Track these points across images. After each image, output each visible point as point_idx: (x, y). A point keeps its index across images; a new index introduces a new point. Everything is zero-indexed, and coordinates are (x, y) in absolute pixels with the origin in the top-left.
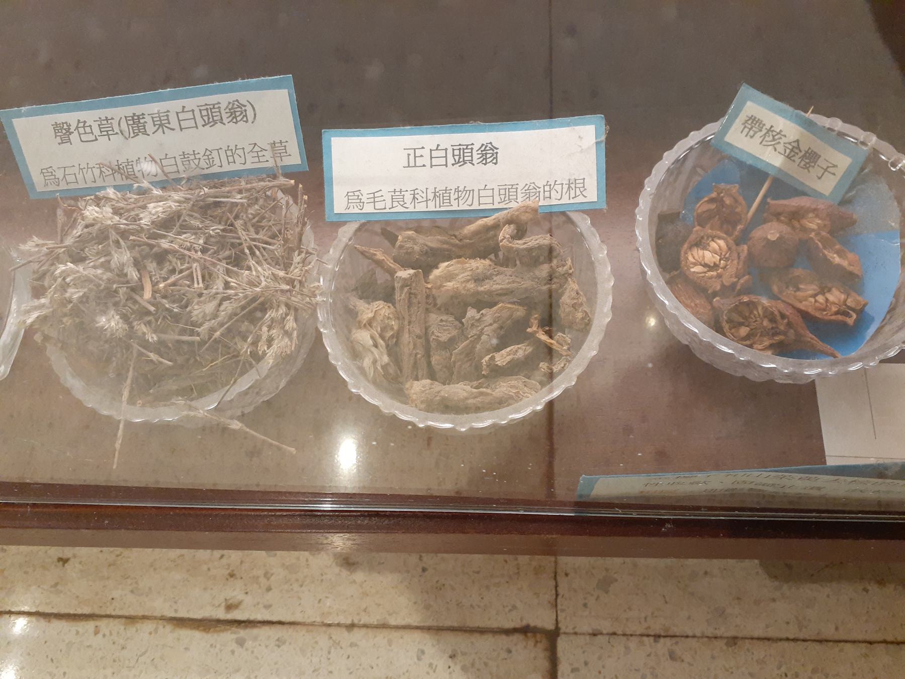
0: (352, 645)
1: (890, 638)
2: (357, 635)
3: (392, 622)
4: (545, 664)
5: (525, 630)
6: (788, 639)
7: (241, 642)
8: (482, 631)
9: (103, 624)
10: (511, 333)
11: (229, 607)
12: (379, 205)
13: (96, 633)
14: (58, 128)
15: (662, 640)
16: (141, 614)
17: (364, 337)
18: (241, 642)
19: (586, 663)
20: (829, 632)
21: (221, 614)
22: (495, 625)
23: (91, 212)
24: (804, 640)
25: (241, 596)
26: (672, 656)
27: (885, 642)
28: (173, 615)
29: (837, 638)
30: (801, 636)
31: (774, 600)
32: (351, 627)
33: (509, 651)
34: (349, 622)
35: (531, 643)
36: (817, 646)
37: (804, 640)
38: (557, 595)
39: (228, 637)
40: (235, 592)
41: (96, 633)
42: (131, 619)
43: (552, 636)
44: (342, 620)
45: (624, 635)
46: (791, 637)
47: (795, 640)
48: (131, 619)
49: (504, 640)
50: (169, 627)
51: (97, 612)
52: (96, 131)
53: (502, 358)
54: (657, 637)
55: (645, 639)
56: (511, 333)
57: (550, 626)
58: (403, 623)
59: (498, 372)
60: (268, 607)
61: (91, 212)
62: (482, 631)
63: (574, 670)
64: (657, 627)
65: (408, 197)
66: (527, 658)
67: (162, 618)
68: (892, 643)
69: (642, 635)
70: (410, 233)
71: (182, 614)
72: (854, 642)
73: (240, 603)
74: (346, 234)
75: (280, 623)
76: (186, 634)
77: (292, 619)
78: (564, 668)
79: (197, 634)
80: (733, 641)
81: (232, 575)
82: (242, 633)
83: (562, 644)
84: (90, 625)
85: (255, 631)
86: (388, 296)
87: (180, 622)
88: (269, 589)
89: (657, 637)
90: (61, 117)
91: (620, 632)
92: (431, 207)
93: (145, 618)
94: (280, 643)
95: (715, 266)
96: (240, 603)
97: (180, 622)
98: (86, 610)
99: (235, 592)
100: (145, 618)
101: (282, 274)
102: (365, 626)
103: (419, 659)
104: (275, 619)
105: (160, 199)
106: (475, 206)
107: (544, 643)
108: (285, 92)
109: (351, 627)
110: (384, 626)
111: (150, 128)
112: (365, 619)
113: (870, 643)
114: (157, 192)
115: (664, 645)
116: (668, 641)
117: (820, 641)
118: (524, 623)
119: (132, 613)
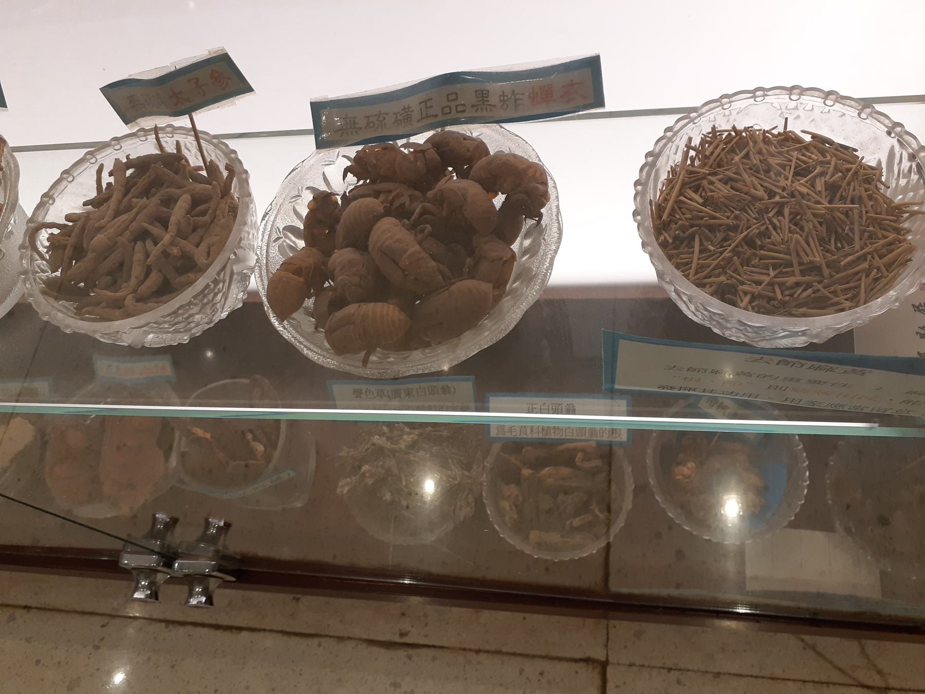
0: (479, 663)
1: (816, 679)
2: (482, 657)
3: (504, 650)
4: (598, 681)
5: (587, 660)
6: (752, 676)
7: (410, 657)
8: (560, 659)
9: (323, 640)
10: (584, 508)
11: (402, 635)
12: (514, 434)
13: (319, 645)
14: (355, 391)
15: (673, 672)
16: (346, 635)
17: (506, 505)
18: (410, 657)
19: (625, 683)
20: (778, 673)
21: (397, 639)
22: (568, 655)
23: (376, 439)
24: (763, 677)
25: (410, 629)
26: (678, 682)
27: (813, 682)
28: (366, 637)
29: (782, 677)
30: (761, 674)
31: (745, 651)
32: (478, 651)
33: (577, 673)
34: (477, 648)
35: (590, 668)
36: (770, 681)
37: (763, 677)
38: (608, 639)
39: (402, 653)
40: (405, 626)
41: (319, 645)
42: (341, 639)
43: (603, 666)
44: (473, 646)
45: (649, 667)
46: (754, 674)
47: (756, 677)
48: (341, 639)
49: (573, 664)
50: (364, 645)
51: (319, 632)
52: (375, 394)
53: (577, 522)
54: (670, 669)
55: (663, 671)
56: (584, 508)
57: (603, 659)
58: (511, 651)
59: (573, 529)
60: (426, 636)
61: (376, 439)
62: (560, 659)
63: (617, 687)
64: (669, 664)
65: (529, 431)
66: (588, 678)
67: (360, 639)
68: (818, 682)
69: (660, 668)
70: (529, 448)
71: (372, 637)
72: (793, 680)
73: (409, 632)
74: (496, 448)
75: (434, 647)
76: (375, 649)
77: (441, 644)
78: (610, 685)
79: (383, 651)
80: (718, 675)
81: (403, 614)
82: (411, 651)
83: (610, 670)
84: (316, 641)
85: (418, 651)
86: (518, 482)
87: (371, 642)
88: (426, 625)
89: (670, 669)
90: (357, 387)
91: (647, 664)
92: (541, 436)
93: (349, 638)
94: (434, 659)
95: (689, 477)
96: (409, 632)
97: (371, 642)
98: (313, 631)
99: (405, 626)
100: (349, 638)
101: (467, 473)
102: (487, 652)
103: (521, 674)
104: (430, 643)
105: (409, 434)
106: (564, 437)
107: (598, 669)
108: (470, 384)
109: (478, 651)
110: (498, 652)
111: (403, 394)
112: (487, 647)
113: (804, 682)
114: (407, 430)
115: (674, 675)
116: (677, 673)
117: (772, 679)
118: (587, 656)
119: (341, 634)
